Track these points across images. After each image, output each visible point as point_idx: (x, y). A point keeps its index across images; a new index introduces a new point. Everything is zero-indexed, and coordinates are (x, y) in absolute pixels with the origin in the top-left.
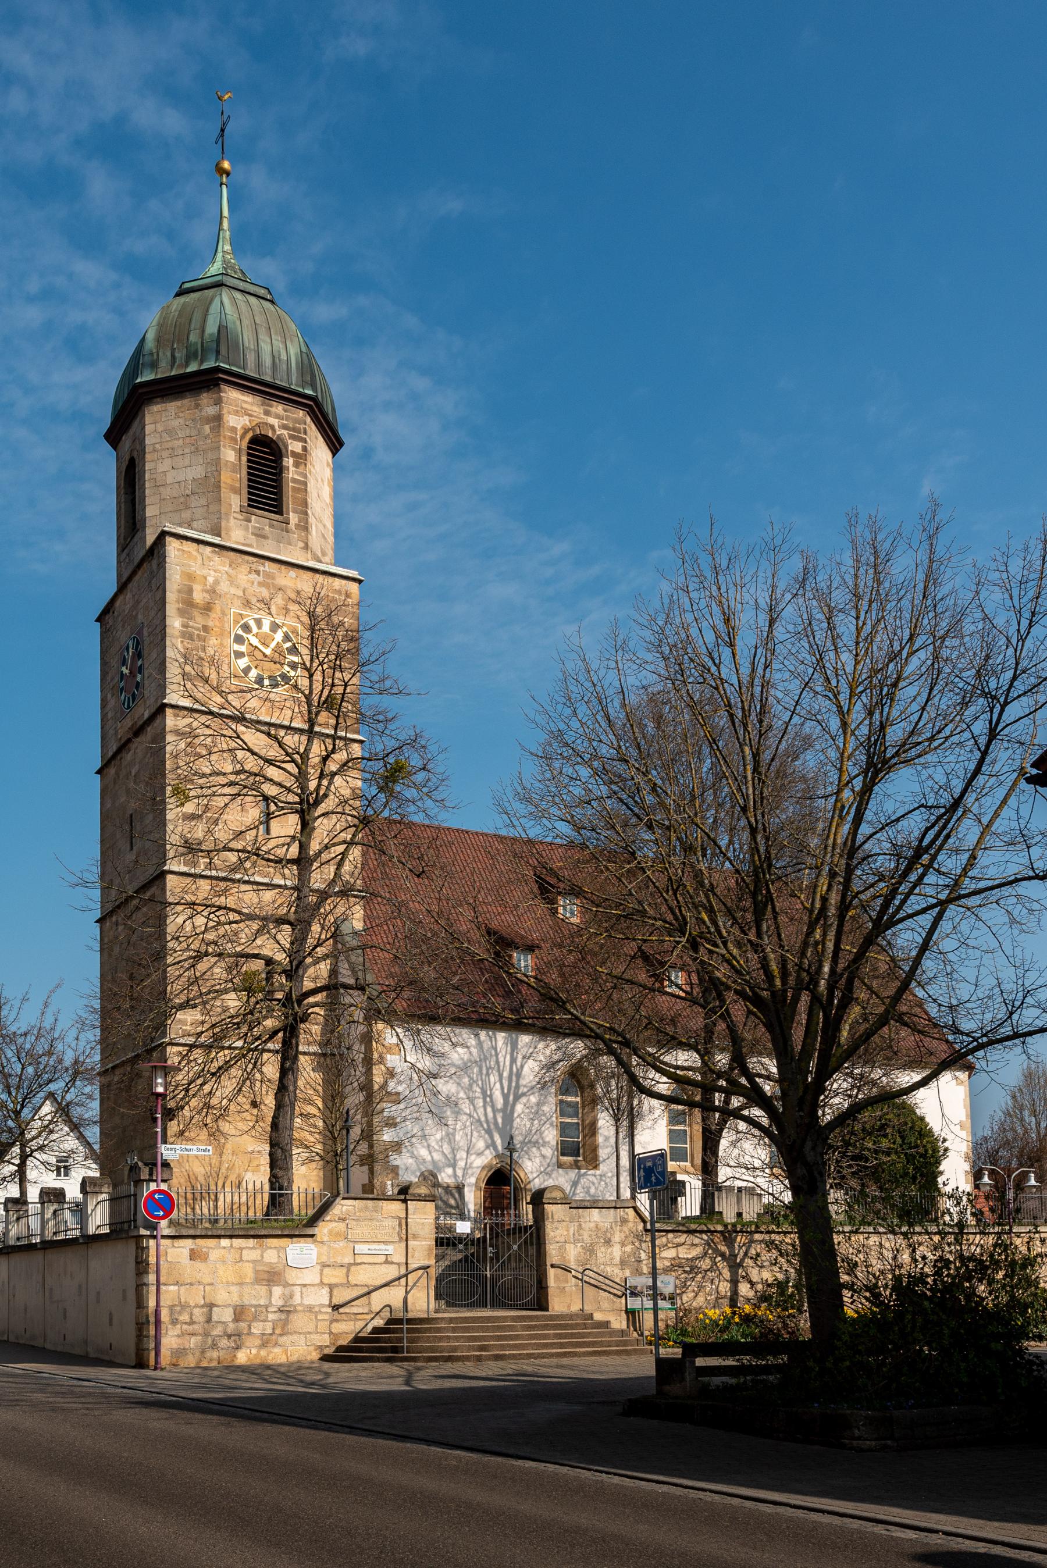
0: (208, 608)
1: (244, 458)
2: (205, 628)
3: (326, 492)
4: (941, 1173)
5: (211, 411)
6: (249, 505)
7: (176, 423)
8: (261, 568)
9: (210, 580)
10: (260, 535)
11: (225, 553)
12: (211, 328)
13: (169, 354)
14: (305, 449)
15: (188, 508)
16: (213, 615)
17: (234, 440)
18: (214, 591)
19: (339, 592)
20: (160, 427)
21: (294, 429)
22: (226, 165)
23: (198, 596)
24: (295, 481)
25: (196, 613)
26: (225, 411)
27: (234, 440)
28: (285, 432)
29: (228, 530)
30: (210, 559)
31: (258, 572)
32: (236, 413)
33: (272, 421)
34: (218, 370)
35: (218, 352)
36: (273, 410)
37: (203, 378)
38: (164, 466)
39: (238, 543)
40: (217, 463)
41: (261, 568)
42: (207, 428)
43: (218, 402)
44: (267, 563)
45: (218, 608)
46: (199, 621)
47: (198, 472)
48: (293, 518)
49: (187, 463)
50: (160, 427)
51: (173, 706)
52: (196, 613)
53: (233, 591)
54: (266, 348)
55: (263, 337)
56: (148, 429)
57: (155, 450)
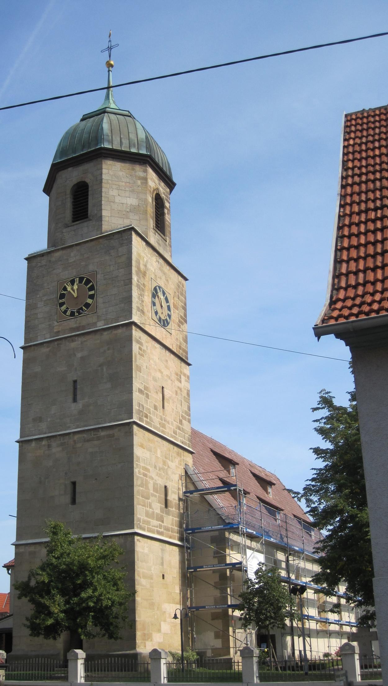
7: (121, 173)
13: (119, 139)
15: (128, 218)
17: (150, 191)
20: (111, 173)
22: (112, 62)
37: (129, 156)
50: (111, 173)
56: (104, 171)
57: (108, 183)
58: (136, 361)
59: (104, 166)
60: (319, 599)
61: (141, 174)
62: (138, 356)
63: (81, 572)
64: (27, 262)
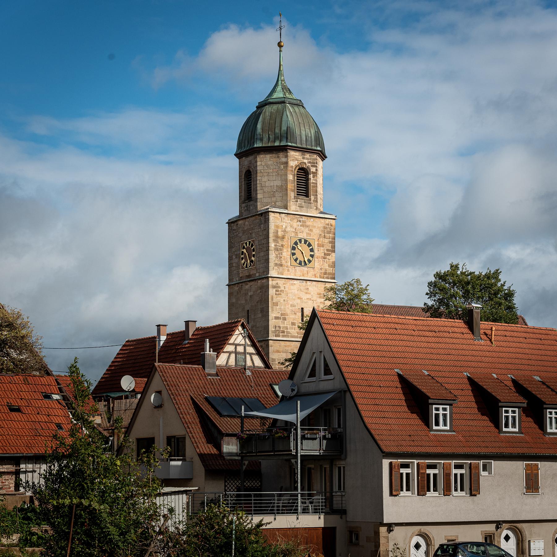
0: (283, 238)
1: (296, 178)
2: (282, 246)
3: (321, 182)
4: (425, 304)
5: (284, 160)
6: (297, 194)
7: (269, 163)
8: (301, 219)
9: (284, 226)
10: (301, 207)
11: (289, 215)
12: (284, 128)
13: (267, 136)
14: (317, 170)
15: (274, 197)
16: (285, 240)
18: (285, 231)
19: (328, 224)
21: (313, 163)
23: (280, 234)
24: (313, 183)
25: (279, 240)
26: (289, 160)
27: (292, 171)
28: (310, 164)
29: (290, 206)
30: (284, 219)
31: (300, 221)
32: (293, 160)
33: (306, 161)
34: (287, 146)
35: (287, 138)
36: (306, 156)
38: (265, 179)
39: (293, 211)
40: (286, 180)
41: (301, 219)
42: (282, 166)
43: (287, 156)
44: (303, 217)
45: (286, 237)
46: (281, 243)
47: (278, 183)
48: (312, 198)
49: (274, 179)
51: (271, 277)
52: (279, 240)
53: (292, 229)
54: (303, 133)
55: (302, 128)
56: (258, 163)
57: (261, 172)
58: (272, 299)
59: (258, 159)
60: (469, 304)
61: (284, 160)
62: (275, 296)
63: (129, 497)
64: (237, 160)
